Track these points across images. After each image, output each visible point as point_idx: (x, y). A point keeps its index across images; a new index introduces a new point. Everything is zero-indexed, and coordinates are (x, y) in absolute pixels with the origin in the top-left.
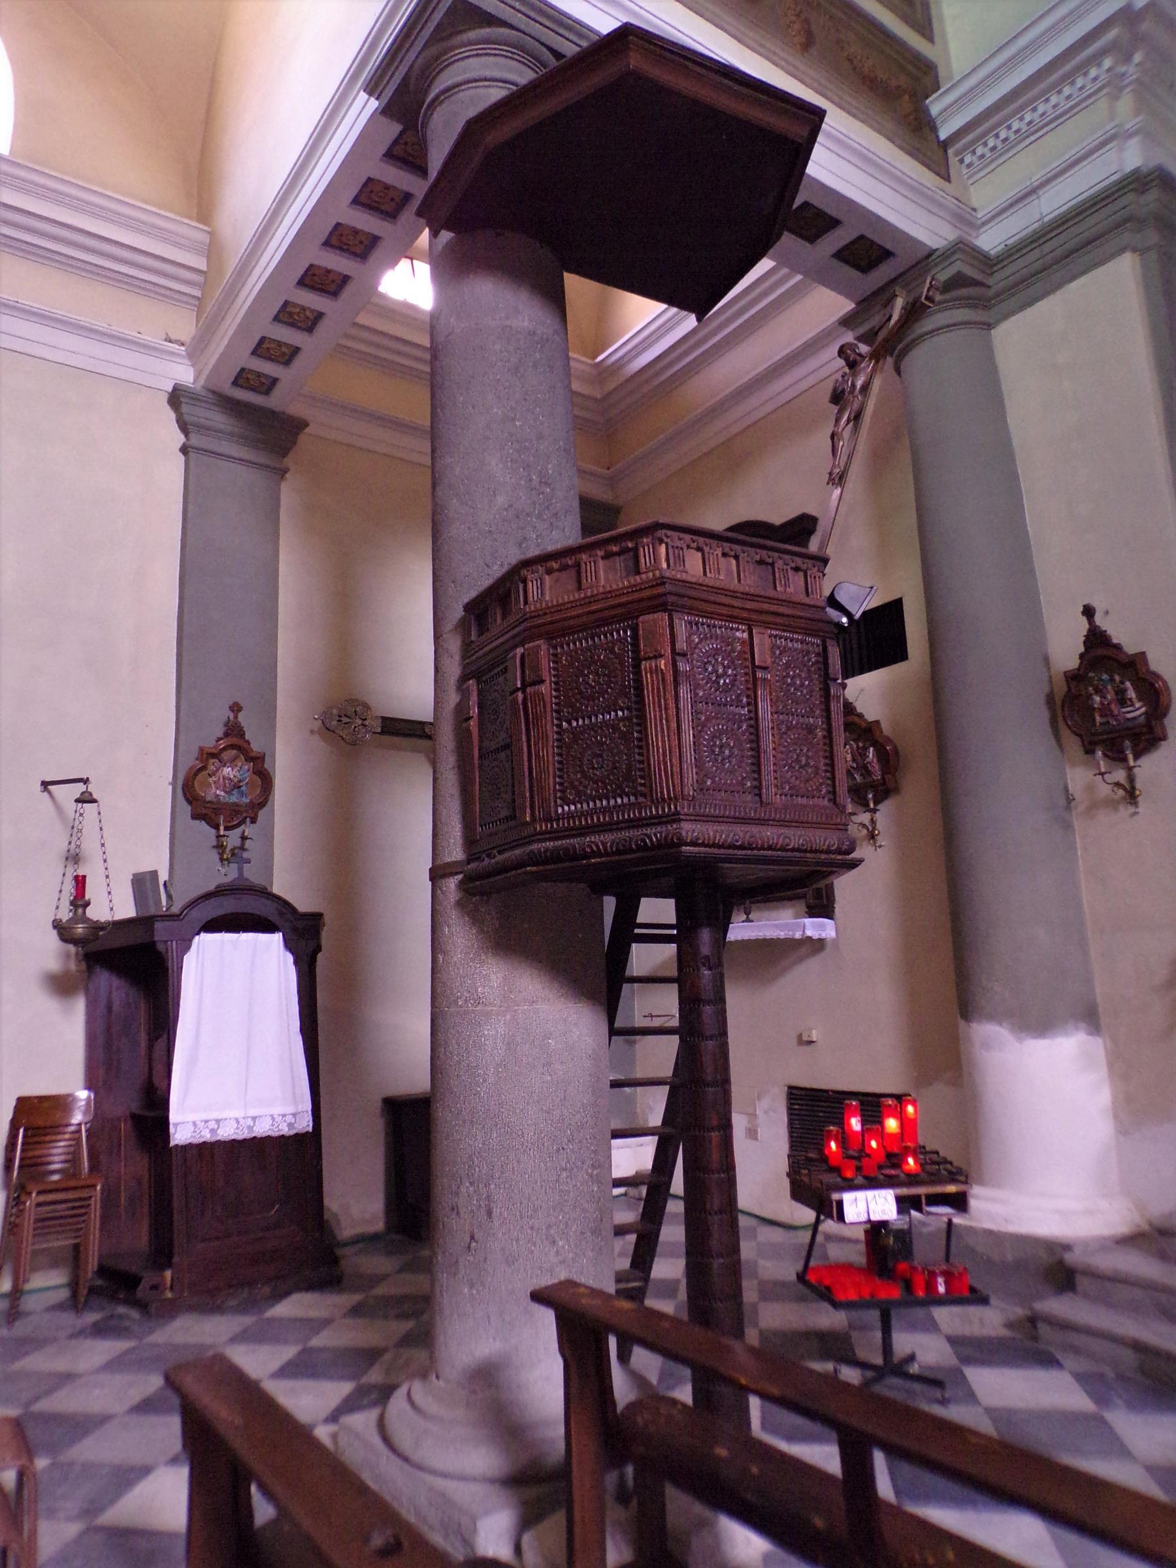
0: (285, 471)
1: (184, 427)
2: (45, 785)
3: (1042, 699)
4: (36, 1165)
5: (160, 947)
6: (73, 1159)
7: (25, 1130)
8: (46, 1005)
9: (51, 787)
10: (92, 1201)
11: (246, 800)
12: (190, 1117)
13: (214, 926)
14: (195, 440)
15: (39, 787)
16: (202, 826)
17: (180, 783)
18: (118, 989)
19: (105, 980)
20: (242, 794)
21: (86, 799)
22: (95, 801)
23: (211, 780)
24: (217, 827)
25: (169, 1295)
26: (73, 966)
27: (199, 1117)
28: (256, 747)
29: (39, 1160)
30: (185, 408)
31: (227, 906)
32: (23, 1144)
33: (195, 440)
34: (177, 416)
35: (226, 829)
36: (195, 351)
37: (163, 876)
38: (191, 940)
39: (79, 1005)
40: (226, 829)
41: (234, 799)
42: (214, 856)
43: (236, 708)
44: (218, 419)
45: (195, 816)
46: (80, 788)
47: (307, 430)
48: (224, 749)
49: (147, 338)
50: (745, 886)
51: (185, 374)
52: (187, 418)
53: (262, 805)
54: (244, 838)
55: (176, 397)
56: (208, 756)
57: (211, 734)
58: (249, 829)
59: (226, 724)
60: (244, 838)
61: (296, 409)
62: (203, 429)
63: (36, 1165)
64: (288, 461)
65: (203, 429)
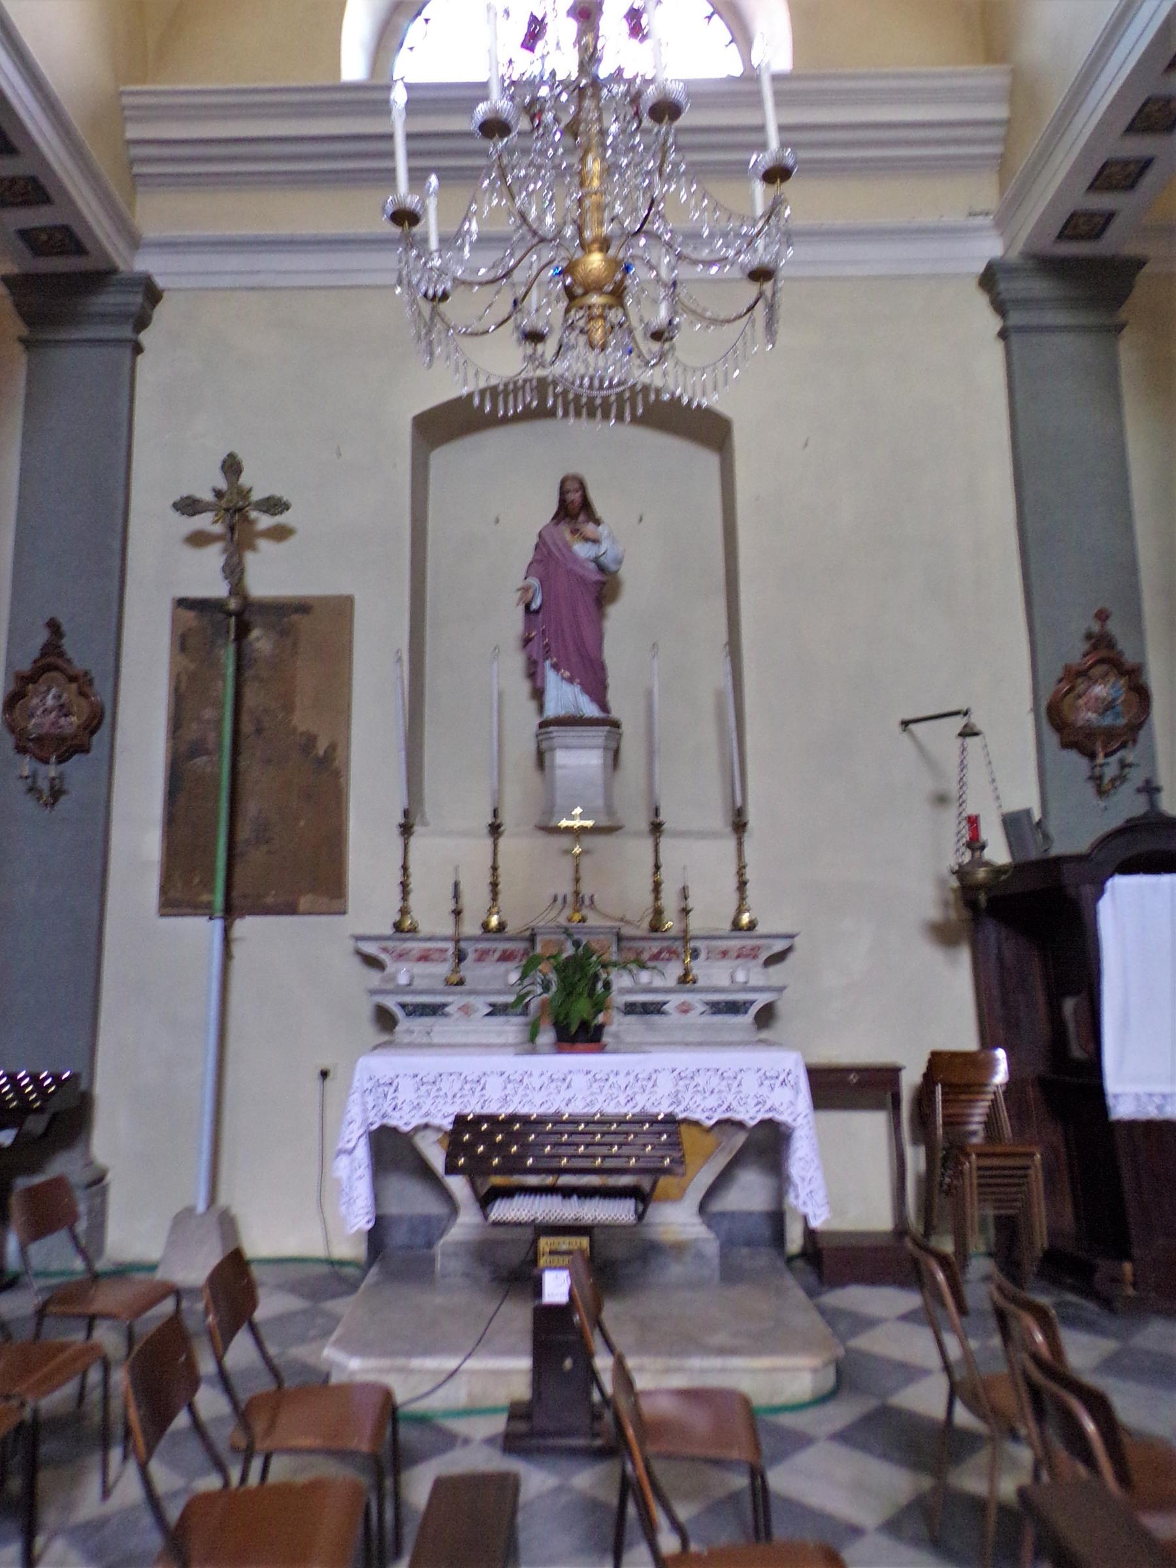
0: (1120, 328)
1: (1000, 307)
2: (906, 724)
3: (559, 481)
4: (959, 1124)
5: (1071, 891)
6: (991, 1123)
7: (942, 1087)
8: (930, 955)
9: (912, 727)
10: (1031, 1172)
11: (1122, 722)
12: (1131, 1088)
13: (1130, 867)
14: (1016, 318)
15: (897, 728)
16: (1073, 756)
17: (1044, 704)
18: (1007, 939)
19: (991, 931)
20: (1117, 715)
21: (968, 732)
22: (976, 734)
23: (1081, 702)
24: (1092, 756)
25: (1130, 1291)
26: (953, 915)
27: (1141, 1089)
28: (1130, 658)
29: (959, 1120)
30: (1002, 286)
31: (1146, 844)
32: (944, 1101)
33: (1016, 318)
34: (991, 297)
35: (1107, 755)
36: (1003, 221)
37: (1037, 816)
38: (1103, 883)
39: (964, 956)
40: (1107, 755)
41: (1108, 721)
42: (1090, 789)
43: (1102, 616)
44: (1040, 287)
45: (1066, 745)
46: (958, 723)
47: (1146, 269)
48: (1091, 667)
49: (362, 230)
50: (995, 922)
51: (991, 248)
52: (1005, 296)
53: (1140, 726)
54: (1123, 765)
55: (989, 279)
56: (1075, 676)
57: (1075, 651)
58: (1130, 755)
59: (1089, 636)
60: (1123, 765)
61: (1131, 249)
62: (1024, 303)
63: (959, 1124)
64: (1123, 314)
65: (1024, 303)
